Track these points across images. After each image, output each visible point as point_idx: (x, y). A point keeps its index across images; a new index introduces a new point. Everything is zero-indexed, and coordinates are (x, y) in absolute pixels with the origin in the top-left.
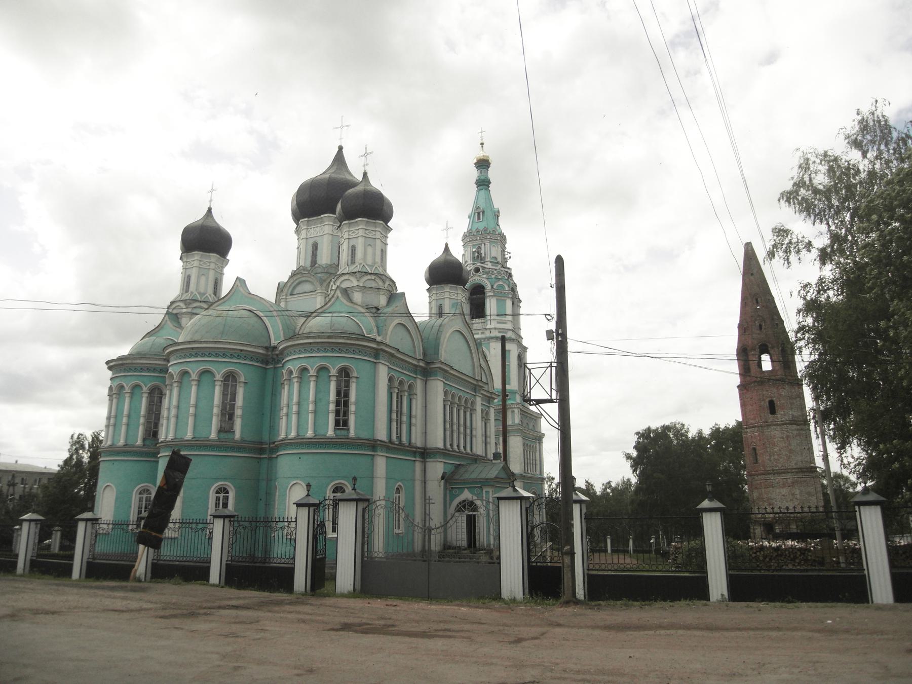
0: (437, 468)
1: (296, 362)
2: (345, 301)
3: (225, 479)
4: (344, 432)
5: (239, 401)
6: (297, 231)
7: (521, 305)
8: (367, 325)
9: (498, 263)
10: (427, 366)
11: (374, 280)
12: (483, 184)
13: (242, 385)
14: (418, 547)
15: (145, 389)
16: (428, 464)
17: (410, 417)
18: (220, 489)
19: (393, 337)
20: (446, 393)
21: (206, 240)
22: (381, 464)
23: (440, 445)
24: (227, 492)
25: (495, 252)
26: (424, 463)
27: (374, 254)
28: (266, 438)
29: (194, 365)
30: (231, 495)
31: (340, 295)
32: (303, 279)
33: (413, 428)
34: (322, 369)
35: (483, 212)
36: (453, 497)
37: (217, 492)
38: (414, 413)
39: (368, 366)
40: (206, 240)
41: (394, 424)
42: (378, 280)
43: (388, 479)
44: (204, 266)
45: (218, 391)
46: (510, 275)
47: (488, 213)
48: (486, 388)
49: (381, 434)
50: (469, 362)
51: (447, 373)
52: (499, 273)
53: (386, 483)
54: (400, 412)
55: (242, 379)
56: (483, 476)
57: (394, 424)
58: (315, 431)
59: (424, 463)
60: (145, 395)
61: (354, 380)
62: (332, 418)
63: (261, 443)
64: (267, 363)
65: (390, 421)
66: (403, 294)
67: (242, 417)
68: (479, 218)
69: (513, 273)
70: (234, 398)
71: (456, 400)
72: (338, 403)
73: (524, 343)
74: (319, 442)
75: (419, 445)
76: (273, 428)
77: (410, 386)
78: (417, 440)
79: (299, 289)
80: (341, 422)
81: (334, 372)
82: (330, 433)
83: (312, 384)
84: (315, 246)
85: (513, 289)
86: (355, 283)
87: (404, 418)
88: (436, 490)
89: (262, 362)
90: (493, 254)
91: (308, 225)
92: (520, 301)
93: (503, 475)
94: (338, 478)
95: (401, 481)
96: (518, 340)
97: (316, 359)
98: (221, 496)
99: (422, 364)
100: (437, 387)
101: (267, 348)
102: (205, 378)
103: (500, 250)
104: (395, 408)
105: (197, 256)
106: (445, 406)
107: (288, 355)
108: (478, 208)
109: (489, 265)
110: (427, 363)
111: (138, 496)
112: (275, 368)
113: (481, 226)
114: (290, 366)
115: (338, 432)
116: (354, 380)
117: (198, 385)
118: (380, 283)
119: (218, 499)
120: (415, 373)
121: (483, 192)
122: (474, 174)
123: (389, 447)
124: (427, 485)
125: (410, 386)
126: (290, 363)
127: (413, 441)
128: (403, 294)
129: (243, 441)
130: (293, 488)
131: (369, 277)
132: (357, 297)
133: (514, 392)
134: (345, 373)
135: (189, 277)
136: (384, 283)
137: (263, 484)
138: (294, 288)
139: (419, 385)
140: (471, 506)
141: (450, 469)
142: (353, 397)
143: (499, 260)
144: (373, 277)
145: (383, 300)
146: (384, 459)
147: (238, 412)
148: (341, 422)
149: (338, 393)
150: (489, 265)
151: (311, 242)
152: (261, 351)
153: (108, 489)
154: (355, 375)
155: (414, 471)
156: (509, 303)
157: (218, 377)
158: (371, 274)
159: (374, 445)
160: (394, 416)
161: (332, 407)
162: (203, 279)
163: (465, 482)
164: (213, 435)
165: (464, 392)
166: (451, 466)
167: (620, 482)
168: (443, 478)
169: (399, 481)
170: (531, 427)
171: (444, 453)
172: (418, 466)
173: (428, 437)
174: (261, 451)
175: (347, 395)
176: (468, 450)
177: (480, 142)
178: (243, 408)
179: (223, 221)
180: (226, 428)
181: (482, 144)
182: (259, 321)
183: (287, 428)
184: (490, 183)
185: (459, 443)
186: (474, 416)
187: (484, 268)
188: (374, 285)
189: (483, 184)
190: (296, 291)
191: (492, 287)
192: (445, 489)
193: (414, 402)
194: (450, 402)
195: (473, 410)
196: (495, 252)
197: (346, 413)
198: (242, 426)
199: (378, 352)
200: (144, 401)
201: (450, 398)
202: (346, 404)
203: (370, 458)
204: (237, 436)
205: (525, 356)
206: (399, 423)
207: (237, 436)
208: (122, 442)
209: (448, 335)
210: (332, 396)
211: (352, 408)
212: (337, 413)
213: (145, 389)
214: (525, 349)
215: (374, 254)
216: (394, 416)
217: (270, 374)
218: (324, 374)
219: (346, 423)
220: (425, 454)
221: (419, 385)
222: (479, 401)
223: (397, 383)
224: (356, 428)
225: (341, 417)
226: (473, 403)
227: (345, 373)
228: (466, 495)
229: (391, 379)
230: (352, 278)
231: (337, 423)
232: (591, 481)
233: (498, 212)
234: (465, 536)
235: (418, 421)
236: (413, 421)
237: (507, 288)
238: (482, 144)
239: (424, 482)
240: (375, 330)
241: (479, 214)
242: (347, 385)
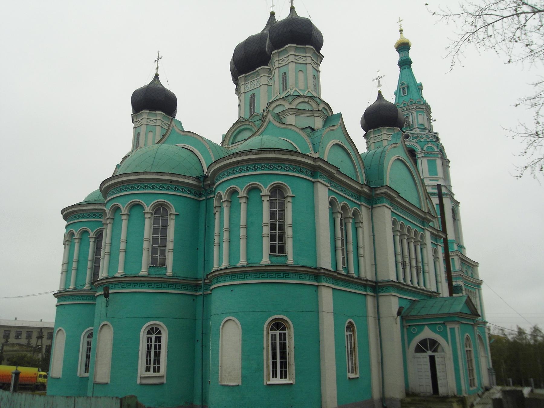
0: (392, 303)
1: (224, 185)
2: (277, 124)
3: (157, 318)
4: (280, 260)
5: (171, 234)
6: (238, 91)
7: (450, 165)
8: (302, 144)
9: (425, 129)
10: (373, 193)
11: (307, 103)
12: (405, 64)
13: (173, 217)
14: (376, 395)
15: (92, 234)
16: (382, 300)
17: (357, 247)
18: (152, 329)
19: (329, 154)
20: (394, 222)
21: (154, 102)
22: (327, 296)
23: (393, 278)
24: (160, 333)
25: (421, 119)
26: (376, 298)
27: (306, 79)
28: (201, 275)
29: (122, 200)
30: (164, 337)
31: (271, 119)
32: (242, 127)
33: (361, 260)
34: (253, 189)
35: (408, 87)
36: (411, 337)
37: (149, 333)
38: (361, 243)
39: (304, 185)
40: (154, 102)
41: (340, 253)
42: (311, 102)
43: (336, 314)
44: (151, 123)
45: (148, 224)
46: (437, 139)
47: (413, 88)
48: (431, 224)
49: (326, 263)
50: (415, 194)
51: (393, 199)
52: (427, 137)
53: (335, 319)
54: (345, 241)
55: (173, 211)
56: (445, 311)
57: (340, 253)
58: (248, 259)
59: (376, 298)
60: (92, 240)
61: (289, 199)
62: (266, 243)
63: (197, 279)
64: (200, 195)
65: (335, 249)
66: (340, 115)
67: (174, 251)
68: (404, 93)
69: (439, 137)
70: (165, 231)
71: (406, 232)
72: (272, 227)
73: (456, 198)
74: (253, 271)
75: (369, 277)
76: (207, 261)
77: (355, 214)
78: (367, 273)
79: (239, 138)
80: (277, 248)
81: (265, 191)
82: (265, 260)
83: (243, 207)
84: (253, 97)
85: (442, 150)
86: (287, 106)
87: (351, 248)
88: (393, 328)
89: (195, 194)
90: (421, 122)
91: (245, 80)
92: (449, 162)
93: (467, 311)
94: (276, 312)
95: (352, 317)
96: (451, 195)
97: (246, 179)
98: (153, 336)
99: (366, 190)
100: (385, 214)
101: (197, 178)
102: (136, 211)
103: (426, 117)
104: (339, 234)
105: (145, 114)
106: (394, 236)
107: (218, 180)
108: (403, 84)
109: (418, 131)
110: (371, 189)
111: (86, 340)
112: (208, 199)
113: (407, 99)
114: (219, 191)
115: (274, 259)
116: (289, 199)
117: (129, 220)
118: (314, 106)
119: (149, 340)
120: (359, 199)
121: (406, 71)
122: (396, 57)
123: (333, 276)
124: (382, 322)
125: (355, 214)
126: (219, 188)
127: (362, 273)
128: (340, 115)
129: (175, 276)
130: (227, 325)
131: (302, 100)
132: (291, 119)
133: (452, 242)
134: (277, 191)
135: (138, 134)
136: (319, 105)
137: (199, 323)
138: (235, 137)
139: (364, 213)
140: (433, 345)
141: (406, 304)
142: (289, 219)
143: (426, 126)
144: (306, 100)
145: (318, 123)
146: (331, 291)
147: (170, 246)
148: (277, 248)
149: (272, 215)
150: (418, 131)
151: (249, 94)
152: (192, 182)
153: (60, 333)
154: (290, 194)
155: (366, 306)
156: (439, 162)
157: (148, 209)
158: (304, 97)
159: (317, 274)
160: (339, 244)
161: (266, 230)
162: (151, 135)
163: (424, 318)
164: (144, 271)
165: (413, 224)
166: (406, 301)
167: (528, 331)
168: (399, 313)
169: (349, 317)
170: (470, 274)
171: (397, 286)
172: (370, 301)
173: (379, 270)
174: (197, 287)
175: (282, 216)
176: (422, 286)
177: (399, 29)
178: (175, 242)
179: (168, 84)
180: (157, 262)
181: (401, 31)
182: (193, 155)
183: (220, 260)
184: (410, 62)
185: (411, 278)
186: (425, 251)
187: (412, 134)
188: (307, 107)
189: (405, 64)
190: (237, 140)
191: (422, 149)
192: (402, 327)
193: (360, 230)
194: (399, 232)
195: (423, 245)
196: (421, 119)
197: (282, 239)
198: (174, 260)
199: (316, 170)
200: (91, 245)
201: (399, 228)
202: (282, 227)
203: (314, 289)
204: (169, 271)
205: (458, 210)
206: (346, 253)
207: (169, 271)
208: (72, 286)
209: (389, 167)
210: (266, 218)
211: (289, 231)
212: (272, 238)
213: (92, 234)
214: (458, 203)
215: (306, 79)
216: (339, 244)
217: (203, 205)
218: (254, 196)
219: (282, 249)
220: (377, 287)
221: (364, 213)
222: (428, 235)
223: (339, 209)
224: (294, 254)
225: (277, 242)
226: (422, 237)
227: (277, 191)
228: (427, 333)
229: (332, 203)
230: (282, 102)
231: (273, 249)
232: (522, 327)
233: (421, 85)
234: (455, 385)
235: (366, 251)
236: (361, 251)
237: (436, 149)
238: (401, 31)
239: (378, 319)
240: (311, 147)
241: (404, 89)
242: (282, 205)
